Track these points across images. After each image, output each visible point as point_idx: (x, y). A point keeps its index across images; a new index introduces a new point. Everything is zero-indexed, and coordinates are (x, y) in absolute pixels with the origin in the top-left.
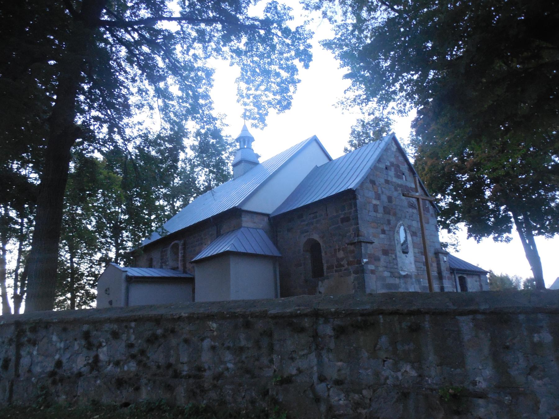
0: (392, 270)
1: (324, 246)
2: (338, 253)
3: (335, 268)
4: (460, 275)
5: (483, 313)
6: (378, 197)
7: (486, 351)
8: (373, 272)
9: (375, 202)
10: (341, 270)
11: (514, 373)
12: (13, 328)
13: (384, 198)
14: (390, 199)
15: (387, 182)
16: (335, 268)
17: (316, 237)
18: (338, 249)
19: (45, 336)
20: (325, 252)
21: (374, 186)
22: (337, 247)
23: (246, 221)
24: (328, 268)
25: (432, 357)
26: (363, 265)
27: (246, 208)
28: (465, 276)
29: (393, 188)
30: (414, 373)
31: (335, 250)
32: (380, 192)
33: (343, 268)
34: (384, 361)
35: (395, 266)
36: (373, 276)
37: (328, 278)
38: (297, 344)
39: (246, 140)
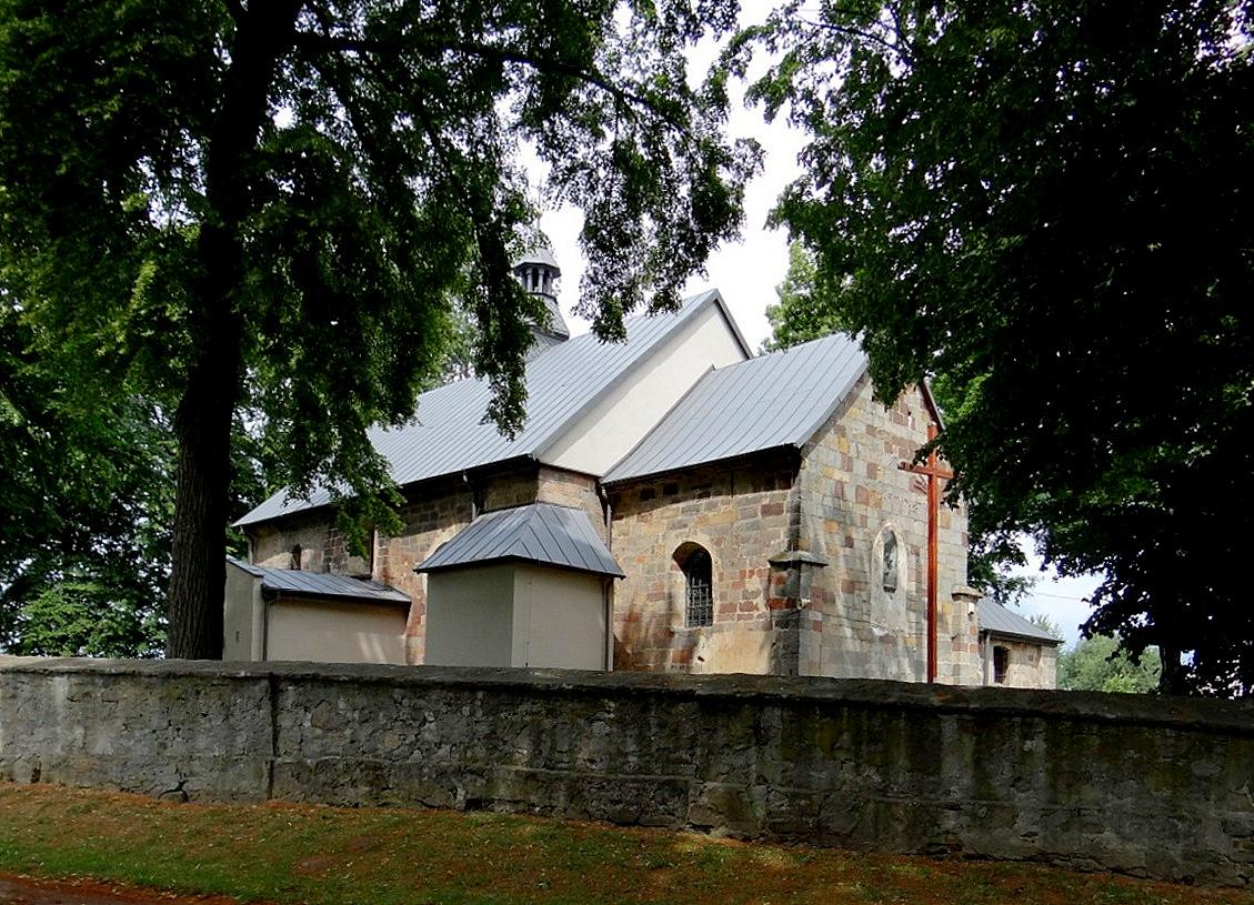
0: (858, 625)
1: (720, 562)
2: (747, 580)
3: (738, 612)
4: (999, 644)
5: (972, 712)
6: (848, 466)
7: (968, 758)
8: (818, 626)
9: (838, 475)
10: (751, 617)
11: (995, 783)
12: (265, 683)
13: (860, 468)
14: (872, 470)
15: (871, 430)
16: (738, 612)
17: (703, 540)
18: (750, 571)
19: (323, 700)
20: (721, 575)
21: (842, 439)
22: (748, 569)
23: (549, 489)
24: (724, 609)
25: (903, 762)
26: (799, 611)
27: (544, 460)
28: (1009, 647)
29: (882, 446)
30: (877, 779)
31: (743, 574)
32: (853, 453)
33: (756, 613)
34: (843, 763)
35: (865, 618)
36: (817, 635)
37: (720, 630)
38: (534, 805)
39: (541, 272)
